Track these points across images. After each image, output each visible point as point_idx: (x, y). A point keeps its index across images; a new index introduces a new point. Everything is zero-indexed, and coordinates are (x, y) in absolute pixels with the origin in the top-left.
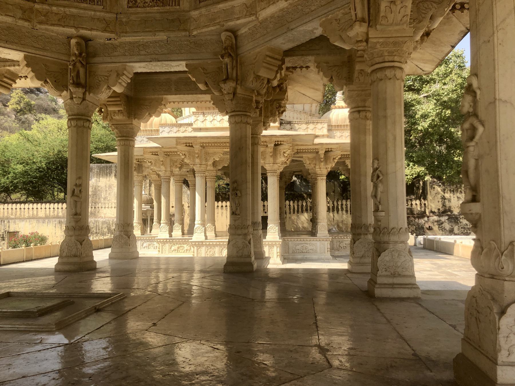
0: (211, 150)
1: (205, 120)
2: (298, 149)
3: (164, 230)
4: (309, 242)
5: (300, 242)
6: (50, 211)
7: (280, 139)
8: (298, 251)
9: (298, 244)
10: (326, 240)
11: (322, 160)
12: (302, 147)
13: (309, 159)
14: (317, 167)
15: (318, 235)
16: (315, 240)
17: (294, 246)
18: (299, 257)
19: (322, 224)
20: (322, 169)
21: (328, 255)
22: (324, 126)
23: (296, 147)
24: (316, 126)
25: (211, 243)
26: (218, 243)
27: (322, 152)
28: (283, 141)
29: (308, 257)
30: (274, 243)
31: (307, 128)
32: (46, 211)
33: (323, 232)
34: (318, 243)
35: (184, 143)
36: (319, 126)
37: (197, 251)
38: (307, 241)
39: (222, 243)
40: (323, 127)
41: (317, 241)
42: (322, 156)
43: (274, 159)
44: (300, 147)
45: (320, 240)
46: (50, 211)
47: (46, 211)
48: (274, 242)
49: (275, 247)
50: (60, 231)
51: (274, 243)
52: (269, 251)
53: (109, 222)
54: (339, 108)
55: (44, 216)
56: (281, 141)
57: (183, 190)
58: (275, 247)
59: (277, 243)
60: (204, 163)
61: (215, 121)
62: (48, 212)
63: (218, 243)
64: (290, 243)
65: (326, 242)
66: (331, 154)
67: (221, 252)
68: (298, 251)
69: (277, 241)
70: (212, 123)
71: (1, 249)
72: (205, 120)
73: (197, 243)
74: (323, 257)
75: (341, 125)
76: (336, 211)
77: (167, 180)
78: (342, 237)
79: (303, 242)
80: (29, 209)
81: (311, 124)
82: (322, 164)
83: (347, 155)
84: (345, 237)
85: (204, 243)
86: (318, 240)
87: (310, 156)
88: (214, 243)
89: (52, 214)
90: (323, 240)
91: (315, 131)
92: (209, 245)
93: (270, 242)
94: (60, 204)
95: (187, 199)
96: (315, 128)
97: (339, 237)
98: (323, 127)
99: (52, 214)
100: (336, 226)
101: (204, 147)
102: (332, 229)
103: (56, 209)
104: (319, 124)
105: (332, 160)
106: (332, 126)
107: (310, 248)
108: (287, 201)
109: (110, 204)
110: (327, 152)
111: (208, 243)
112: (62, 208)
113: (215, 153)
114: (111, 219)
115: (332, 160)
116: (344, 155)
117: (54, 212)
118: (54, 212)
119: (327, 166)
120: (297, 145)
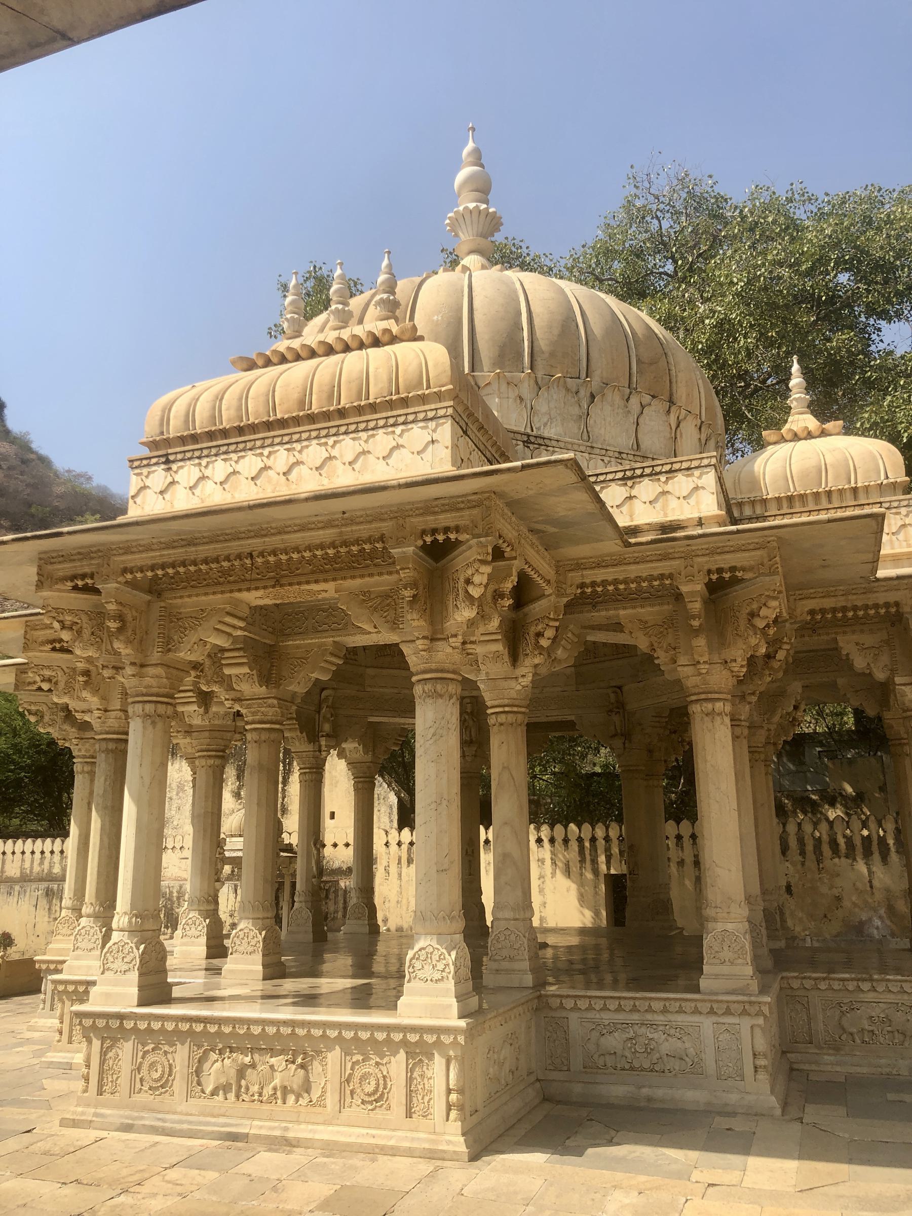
0: (188, 602)
1: (173, 483)
2: (582, 586)
3: (193, 932)
4: (660, 1018)
5: (621, 1017)
6: (32, 862)
7: (445, 519)
8: (610, 1061)
9: (614, 1028)
10: (744, 1013)
11: (696, 623)
12: (600, 575)
13: (644, 625)
14: (682, 660)
15: (703, 983)
16: (689, 1006)
17: (595, 1034)
18: (618, 1091)
19: (720, 927)
20: (704, 668)
21: (761, 1091)
22: (700, 483)
23: (576, 577)
24: (668, 488)
25: (156, 1026)
26: (184, 1027)
27: (693, 589)
28: (457, 529)
29: (659, 1093)
30: (430, 1039)
31: (631, 498)
32: (23, 860)
33: (725, 969)
34: (707, 1024)
35: (64, 579)
36: (681, 483)
37: (102, 1062)
38: (650, 1010)
39: (199, 1028)
40: (697, 488)
41: (696, 1012)
42: (696, 606)
43: (432, 623)
44: (591, 576)
45: (712, 1012)
46: (32, 862)
47: (23, 860)
48: (431, 1030)
49: (439, 1061)
50: (46, 919)
51: (430, 1039)
52: (410, 1080)
53: (171, 893)
54: (796, 437)
55: (18, 875)
56: (446, 530)
57: (377, 791)
58: (439, 1061)
59: (447, 1039)
60: (155, 656)
61: (209, 484)
62: (27, 865)
63: (184, 1027)
64: (574, 1017)
65: (745, 1024)
66: (738, 594)
67: (198, 1072)
68: (610, 1061)
69: (447, 1030)
70: (197, 492)
71: (2, 957)
72: (173, 483)
73: (101, 1023)
74: (733, 1098)
75: (802, 497)
76: (876, 856)
77: (111, 746)
78: (851, 986)
79: (636, 1017)
80: (23, 853)
81: (646, 481)
82: (701, 642)
83: (834, 610)
84: (866, 986)
85: (129, 1024)
86: (705, 1007)
87: (649, 612)
88: (170, 1026)
89: (36, 869)
90: (728, 1012)
91: (664, 508)
92: (149, 1030)
93: (413, 1029)
94: (39, 841)
95: (387, 820)
96: (664, 493)
97: (836, 985)
98: (697, 488)
99: (36, 869)
100: (882, 911)
101: (159, 595)
102: (870, 919)
103: (48, 854)
104: (680, 478)
105: (743, 623)
106: (764, 502)
107: (667, 1046)
108: (671, 822)
109: (179, 838)
110: (719, 587)
111: (143, 1025)
112: (13, 853)
113: (200, 617)
114: (176, 884)
115: (743, 623)
116: (823, 611)
117: (42, 863)
118: (42, 863)
119: (729, 654)
120: (578, 565)
